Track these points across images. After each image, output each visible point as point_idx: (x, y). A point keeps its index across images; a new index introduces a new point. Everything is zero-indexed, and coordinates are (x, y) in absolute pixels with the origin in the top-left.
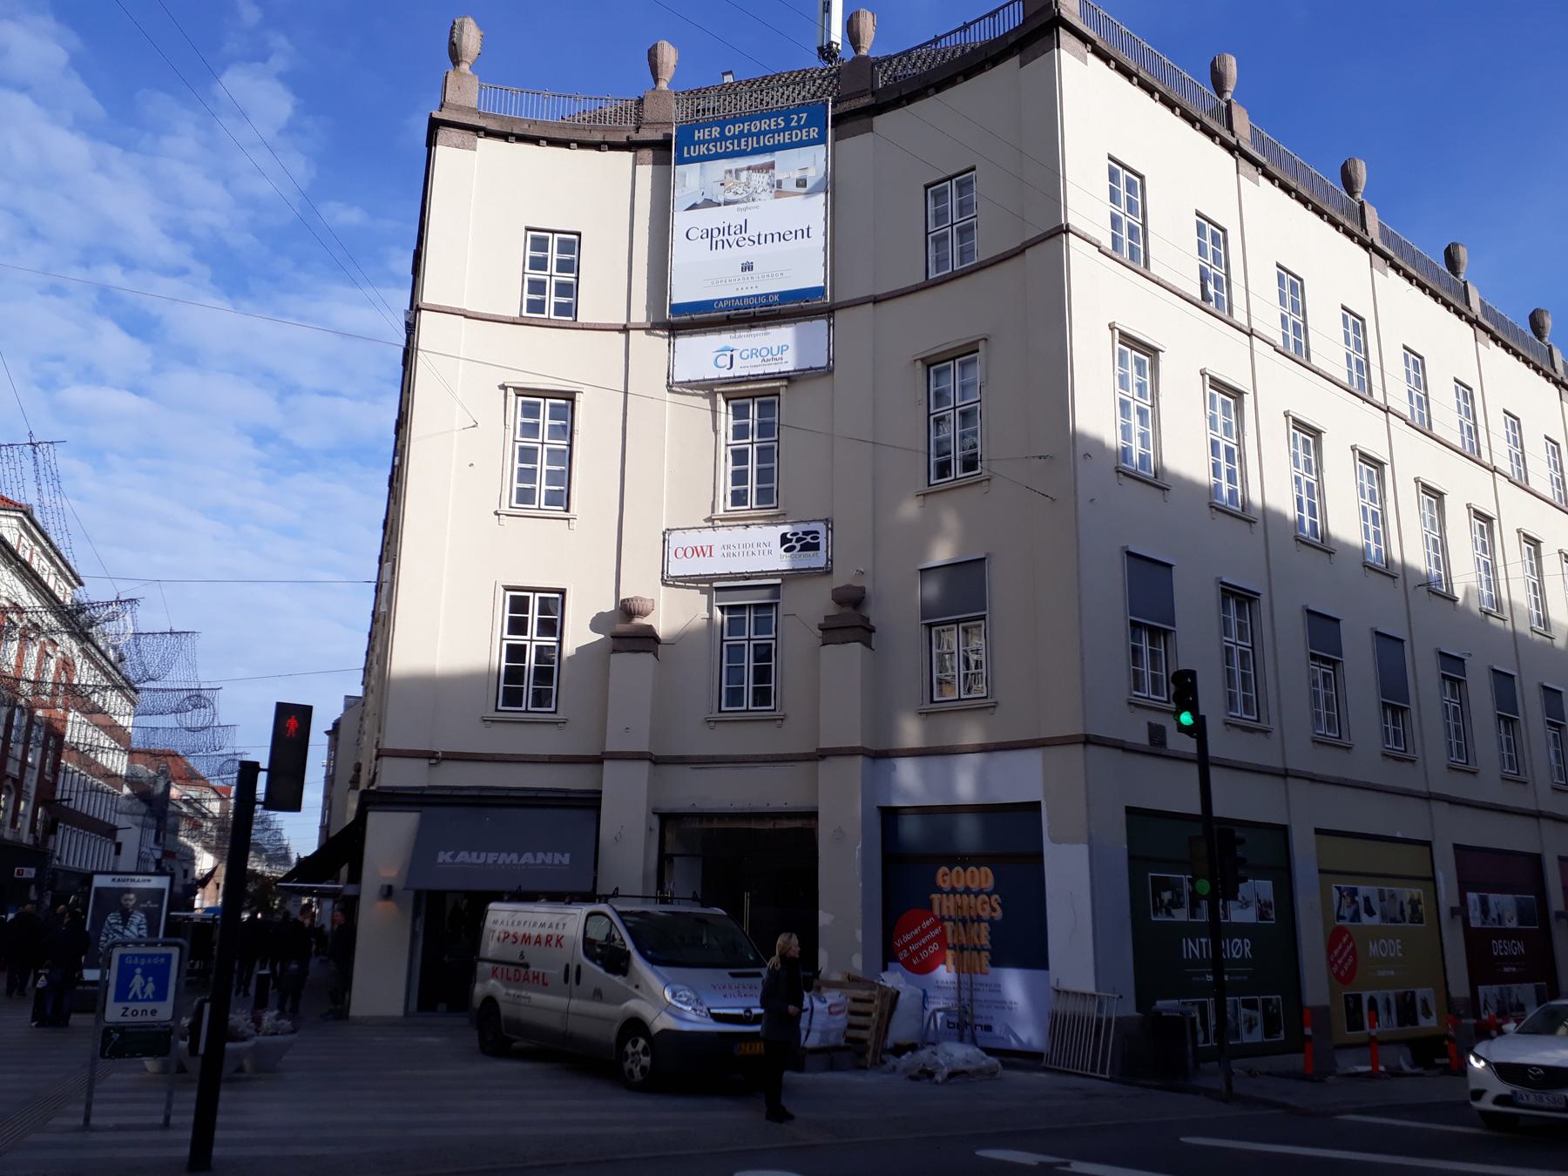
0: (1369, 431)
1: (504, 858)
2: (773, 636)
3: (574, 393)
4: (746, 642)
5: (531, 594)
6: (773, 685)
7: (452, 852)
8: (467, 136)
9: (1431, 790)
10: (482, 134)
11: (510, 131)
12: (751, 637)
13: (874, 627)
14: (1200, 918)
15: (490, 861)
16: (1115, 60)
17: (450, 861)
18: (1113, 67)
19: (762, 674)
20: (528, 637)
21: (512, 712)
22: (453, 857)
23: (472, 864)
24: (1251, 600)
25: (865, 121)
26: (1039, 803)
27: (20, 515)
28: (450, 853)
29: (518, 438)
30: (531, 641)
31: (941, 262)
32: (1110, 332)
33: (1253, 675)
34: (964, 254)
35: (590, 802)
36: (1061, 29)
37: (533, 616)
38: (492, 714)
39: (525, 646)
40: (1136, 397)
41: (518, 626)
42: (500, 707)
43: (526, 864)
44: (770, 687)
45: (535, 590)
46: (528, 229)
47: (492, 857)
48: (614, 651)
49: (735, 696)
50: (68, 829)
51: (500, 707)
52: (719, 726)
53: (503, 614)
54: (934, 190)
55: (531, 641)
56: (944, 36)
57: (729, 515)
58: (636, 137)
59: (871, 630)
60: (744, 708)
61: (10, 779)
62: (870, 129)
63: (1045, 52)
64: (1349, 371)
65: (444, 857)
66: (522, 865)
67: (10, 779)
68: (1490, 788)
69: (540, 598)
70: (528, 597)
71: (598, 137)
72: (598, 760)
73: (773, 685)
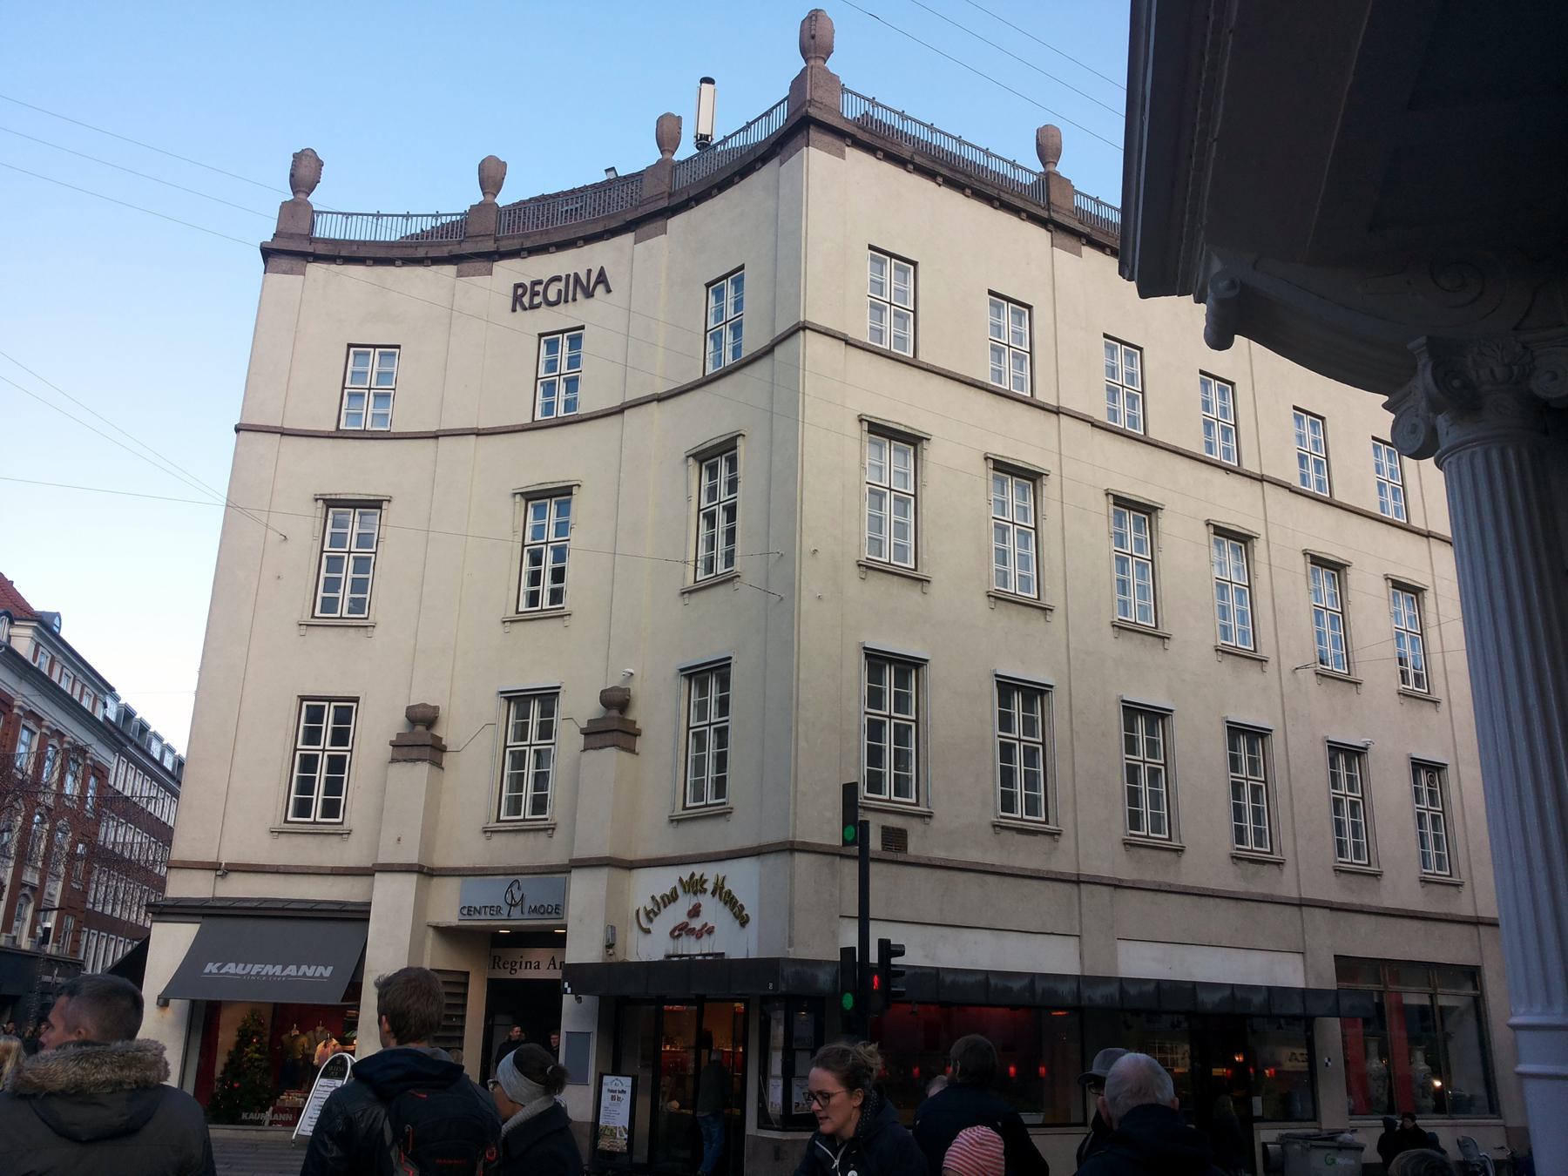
1: (269, 969)
2: (349, 748)
4: (321, 753)
5: (327, 704)
6: (343, 798)
7: (220, 964)
8: (296, 263)
9: (1479, 915)
10: (311, 259)
11: (337, 254)
12: (326, 748)
13: (640, 730)
18: (881, 157)
20: (321, 747)
22: (219, 968)
25: (660, 223)
27: (35, 625)
28: (218, 965)
33: (1359, 777)
35: (358, 915)
37: (328, 725)
38: (493, 825)
39: (318, 755)
40: (1312, 452)
41: (312, 736)
42: (290, 818)
43: (289, 976)
44: (340, 800)
45: (330, 700)
46: (350, 346)
47: (257, 968)
48: (393, 761)
49: (303, 808)
50: (121, 941)
51: (289, 818)
52: (281, 835)
56: (731, 137)
59: (636, 734)
60: (311, 819)
61: (28, 888)
63: (798, 151)
64: (1206, 442)
65: (211, 968)
66: (282, 977)
67: (28, 888)
69: (335, 707)
70: (324, 706)
71: (599, 228)
72: (368, 872)
73: (343, 798)
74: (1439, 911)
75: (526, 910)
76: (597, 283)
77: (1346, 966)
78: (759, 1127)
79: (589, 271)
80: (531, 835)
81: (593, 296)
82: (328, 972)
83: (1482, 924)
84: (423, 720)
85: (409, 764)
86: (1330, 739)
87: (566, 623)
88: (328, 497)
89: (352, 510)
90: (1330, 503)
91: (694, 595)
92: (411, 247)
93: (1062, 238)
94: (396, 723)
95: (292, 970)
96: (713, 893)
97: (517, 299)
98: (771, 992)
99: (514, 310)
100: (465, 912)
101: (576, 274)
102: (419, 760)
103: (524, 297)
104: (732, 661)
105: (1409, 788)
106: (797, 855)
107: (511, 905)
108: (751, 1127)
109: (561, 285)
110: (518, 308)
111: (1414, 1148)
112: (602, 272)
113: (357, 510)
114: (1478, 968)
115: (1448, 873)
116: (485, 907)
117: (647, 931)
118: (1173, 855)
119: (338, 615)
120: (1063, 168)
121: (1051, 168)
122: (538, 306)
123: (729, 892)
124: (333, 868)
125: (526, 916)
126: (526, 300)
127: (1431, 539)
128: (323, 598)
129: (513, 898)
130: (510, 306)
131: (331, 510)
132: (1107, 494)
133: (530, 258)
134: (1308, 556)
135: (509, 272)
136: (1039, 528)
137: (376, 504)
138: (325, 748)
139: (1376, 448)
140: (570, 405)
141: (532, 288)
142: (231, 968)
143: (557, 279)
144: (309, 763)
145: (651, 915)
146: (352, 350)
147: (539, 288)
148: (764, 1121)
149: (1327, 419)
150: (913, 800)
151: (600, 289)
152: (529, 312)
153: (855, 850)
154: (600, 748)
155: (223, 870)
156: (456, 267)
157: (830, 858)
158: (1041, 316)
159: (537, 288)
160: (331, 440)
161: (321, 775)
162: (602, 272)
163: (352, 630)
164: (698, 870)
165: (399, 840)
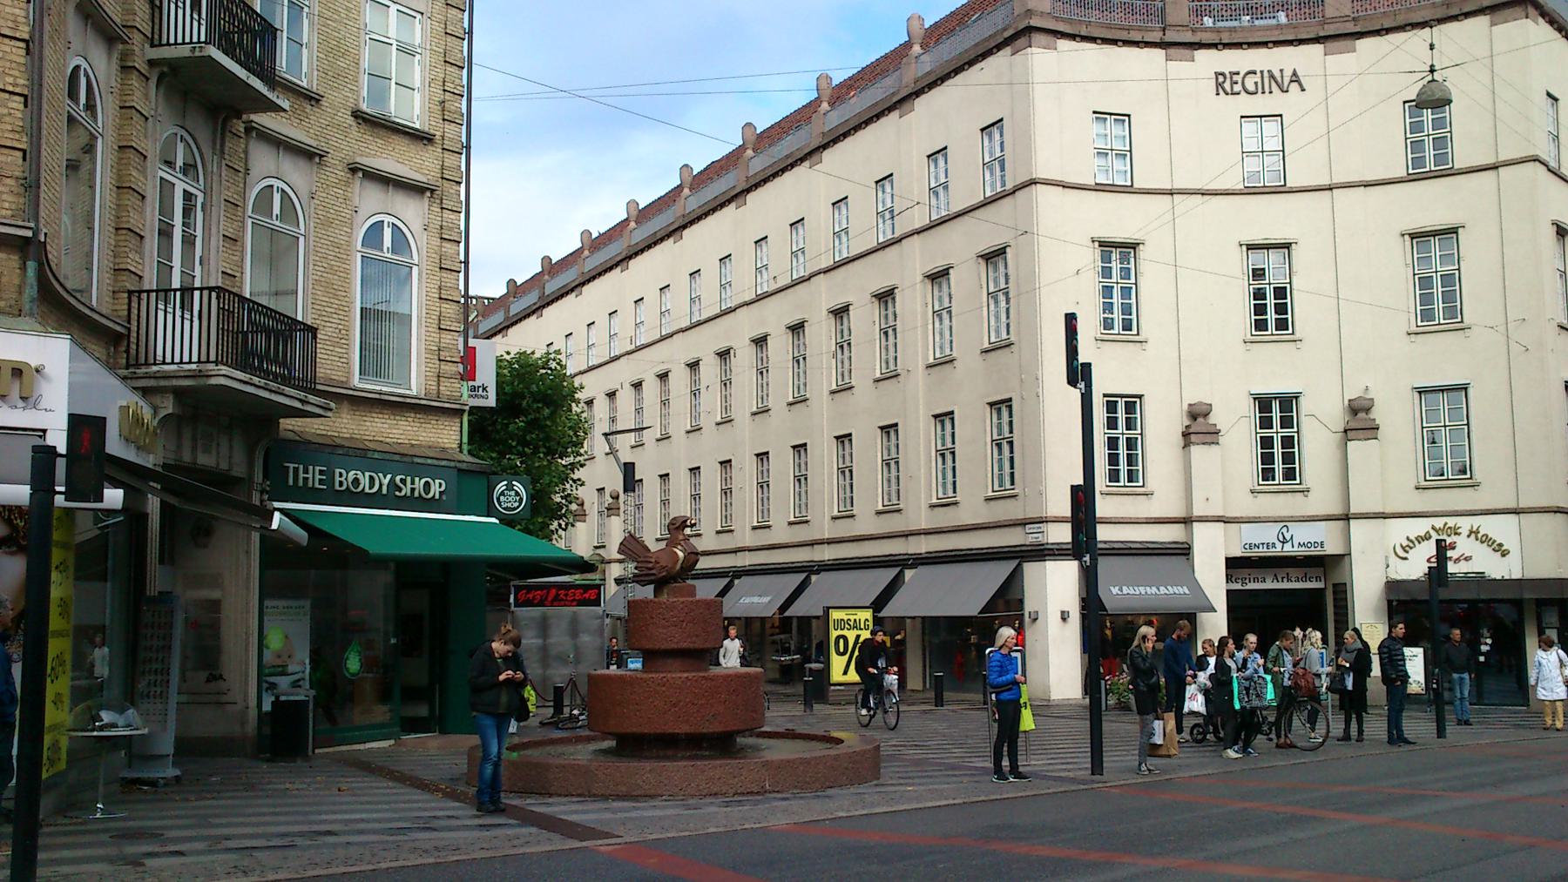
3: (1291, 244)
5: (1119, 399)
10: (1197, 47)
21: (1269, 486)
24: (1297, 398)
26: (102, 501)
29: (1251, 282)
30: (1277, 433)
31: (1418, 162)
34: (1440, 158)
35: (1184, 551)
45: (1122, 396)
46: (1405, 102)
55: (1277, 433)
57: (1421, 329)
71: (1401, 20)
72: (1187, 521)
75: (1296, 545)
84: (1197, 414)
85: (1206, 446)
87: (1467, 335)
89: (1432, 238)
94: (1179, 422)
97: (1219, 85)
100: (1247, 546)
103: (1224, 83)
107: (1283, 543)
109: (1257, 78)
111: (416, 733)
112: (1295, 74)
113: (1437, 238)
117: (1406, 559)
119: (1437, 322)
125: (1296, 549)
126: (1227, 86)
131: (1415, 241)
137: (1453, 231)
138: (1277, 432)
140: (1440, 158)
141: (1231, 78)
143: (1254, 73)
144: (1267, 443)
145: (1407, 549)
146: (1407, 105)
147: (1238, 78)
150: (1298, 481)
151: (1294, 87)
152: (1230, 96)
159: (1235, 78)
161: (1278, 450)
162: (1295, 74)
164: (1451, 522)
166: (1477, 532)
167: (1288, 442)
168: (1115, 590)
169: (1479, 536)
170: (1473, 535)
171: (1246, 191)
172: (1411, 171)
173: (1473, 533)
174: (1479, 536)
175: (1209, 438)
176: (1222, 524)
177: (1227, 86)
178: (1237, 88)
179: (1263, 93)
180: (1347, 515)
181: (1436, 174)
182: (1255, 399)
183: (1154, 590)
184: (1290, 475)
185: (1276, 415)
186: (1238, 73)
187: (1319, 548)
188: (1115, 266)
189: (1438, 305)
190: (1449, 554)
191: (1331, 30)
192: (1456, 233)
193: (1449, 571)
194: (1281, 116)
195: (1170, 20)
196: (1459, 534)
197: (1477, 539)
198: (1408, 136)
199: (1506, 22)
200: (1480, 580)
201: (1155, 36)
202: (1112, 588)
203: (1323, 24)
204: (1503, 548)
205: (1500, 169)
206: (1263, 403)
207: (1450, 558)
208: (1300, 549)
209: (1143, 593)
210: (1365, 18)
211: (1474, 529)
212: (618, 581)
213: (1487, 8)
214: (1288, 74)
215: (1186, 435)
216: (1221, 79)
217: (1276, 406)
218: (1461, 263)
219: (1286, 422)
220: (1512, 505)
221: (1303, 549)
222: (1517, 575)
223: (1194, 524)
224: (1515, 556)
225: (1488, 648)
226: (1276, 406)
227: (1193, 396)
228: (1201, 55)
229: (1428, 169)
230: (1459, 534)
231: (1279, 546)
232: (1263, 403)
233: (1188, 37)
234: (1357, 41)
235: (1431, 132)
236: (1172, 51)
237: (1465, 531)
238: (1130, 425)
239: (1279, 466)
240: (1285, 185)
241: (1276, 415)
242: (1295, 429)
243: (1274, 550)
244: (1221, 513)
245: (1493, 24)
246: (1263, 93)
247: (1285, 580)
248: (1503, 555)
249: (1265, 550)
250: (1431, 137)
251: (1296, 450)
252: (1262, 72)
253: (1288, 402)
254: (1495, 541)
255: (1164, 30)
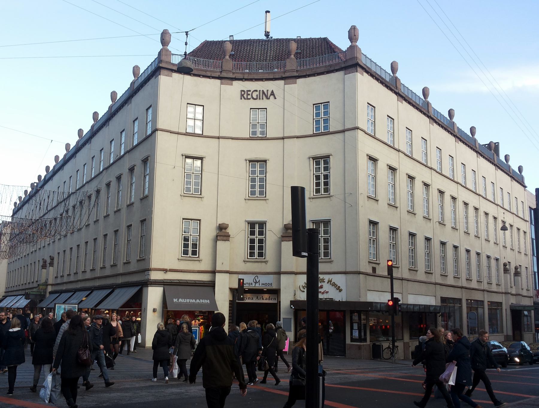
0: (392, 158)
2: (329, 235)
10: (174, 72)
14: (324, 357)
15: (188, 302)
16: (370, 73)
17: (177, 301)
19: (261, 248)
23: (183, 302)
25: (294, 80)
30: (257, 237)
31: (318, 129)
32: (186, 36)
34: (326, 127)
35: (212, 285)
36: (358, 66)
38: (180, 258)
46: (314, 105)
47: (188, 300)
53: (247, 229)
54: (317, 106)
55: (257, 237)
58: (221, 76)
62: (296, 83)
68: (450, 281)
74: (468, 286)
75: (261, 284)
76: (271, 95)
77: (444, 300)
78: (351, 342)
79: (268, 91)
80: (260, 263)
81: (269, 99)
82: (208, 301)
83: (464, 288)
85: (224, 242)
86: (410, 231)
88: (187, 155)
90: (411, 158)
91: (314, 199)
92: (204, 71)
93: (400, 99)
95: (198, 301)
96: (328, 283)
97: (242, 95)
98: (397, 309)
99: (241, 99)
101: (263, 91)
102: (227, 240)
103: (244, 95)
104: (331, 220)
105: (367, 230)
106: (361, 275)
107: (256, 283)
108: (348, 341)
109: (258, 93)
110: (243, 98)
112: (272, 92)
113: (259, 163)
114: (461, 299)
115: (376, 260)
116: (247, 283)
118: (416, 272)
119: (256, 196)
120: (398, 75)
121: (354, 44)
122: (250, 99)
123: (334, 283)
124: (198, 271)
125: (261, 286)
126: (245, 96)
127: (400, 152)
128: (186, 187)
129: (256, 281)
130: (240, 98)
131: (250, 163)
132: (387, 165)
133: (245, 82)
134: (368, 156)
135: (238, 86)
136: (395, 184)
138: (257, 237)
139: (368, 106)
141: (247, 93)
142: (180, 300)
143: (256, 91)
144: (252, 241)
146: (314, 106)
148: (352, 340)
149: (395, 120)
151: (272, 97)
152: (246, 100)
153: (389, 276)
154: (289, 241)
155: (165, 271)
156: (220, 81)
157: (365, 275)
158: (396, 121)
159: (249, 93)
160: (185, 136)
161: (256, 245)
162: (272, 92)
163: (197, 198)
165: (223, 263)
166: (331, 281)
167: (261, 241)
168: (175, 300)
169: (332, 283)
170: (329, 283)
171: (250, 138)
172: (251, 136)
173: (329, 281)
174: (332, 283)
175: (225, 238)
176: (228, 274)
177: (245, 96)
178: (249, 97)
179: (260, 99)
180: (214, 271)
181: (324, 134)
182: (248, 223)
183: (194, 301)
184: (261, 255)
185: (257, 230)
186: (250, 91)
187: (270, 286)
188: (258, 169)
189: (322, 187)
190: (320, 290)
191: (287, 74)
192: (329, 157)
193: (319, 297)
194: (266, 109)
195: (224, 68)
196: (324, 282)
197: (331, 284)
198: (315, 118)
199: (350, 73)
200: (331, 301)
201: (217, 75)
202: (174, 299)
203: (285, 72)
204: (340, 288)
205: (346, 132)
206: (252, 225)
207: (320, 292)
208: (263, 286)
209: (188, 302)
210: (301, 71)
211: (330, 280)
212: (51, 293)
213: (344, 68)
214: (269, 93)
215: (217, 236)
216: (243, 93)
217: (257, 226)
218: (267, 174)
219: (261, 233)
220: (343, 270)
221: (264, 286)
222: (344, 300)
223: (152, 271)
224: (344, 291)
225: (332, 331)
226: (257, 226)
227: (220, 222)
228: (235, 83)
229: (257, 136)
230: (324, 282)
231: (254, 284)
232: (252, 225)
233: (231, 75)
234: (297, 80)
235: (323, 117)
236: (223, 81)
237: (326, 281)
238: (261, 233)
239: (256, 251)
240: (266, 137)
241: (257, 230)
242: (264, 236)
243: (252, 286)
244: (228, 270)
245: (345, 74)
246: (260, 99)
247: (261, 299)
248: (340, 291)
249: (248, 286)
250: (322, 119)
251: (264, 245)
252: (260, 91)
253: (262, 225)
254: (337, 285)
255: (221, 72)
